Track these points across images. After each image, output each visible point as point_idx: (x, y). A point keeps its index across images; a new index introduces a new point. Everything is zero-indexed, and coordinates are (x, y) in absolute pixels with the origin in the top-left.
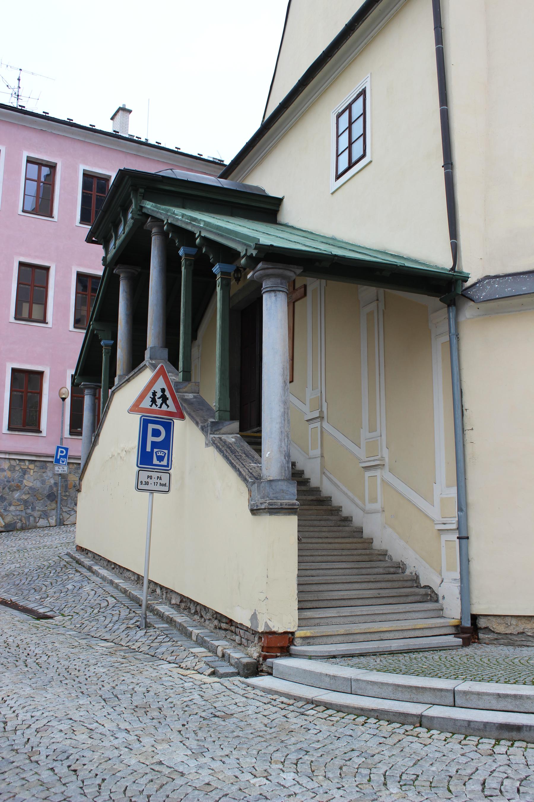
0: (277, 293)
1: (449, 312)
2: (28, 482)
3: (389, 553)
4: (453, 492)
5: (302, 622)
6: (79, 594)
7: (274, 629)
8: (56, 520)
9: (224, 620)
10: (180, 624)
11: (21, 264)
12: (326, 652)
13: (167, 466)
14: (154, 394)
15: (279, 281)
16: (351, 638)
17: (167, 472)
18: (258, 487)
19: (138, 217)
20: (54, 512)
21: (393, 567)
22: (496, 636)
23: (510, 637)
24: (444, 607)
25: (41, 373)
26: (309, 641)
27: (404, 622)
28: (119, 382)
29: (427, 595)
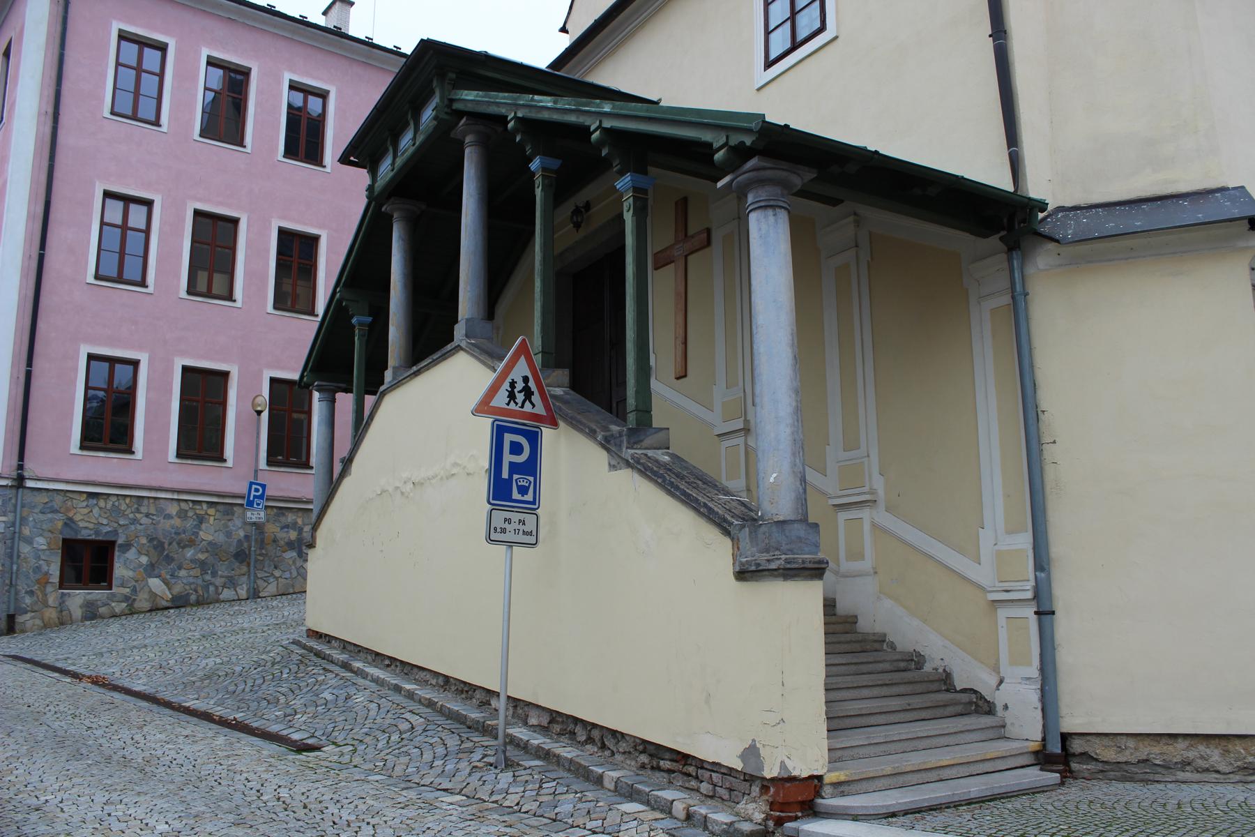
0: (778, 210)
1: (1010, 261)
2: (207, 534)
3: (890, 638)
4: (1024, 541)
5: (836, 756)
6: (350, 709)
7: (795, 773)
8: (248, 590)
9: (667, 756)
10: (571, 761)
11: (197, 213)
12: (882, 807)
13: (534, 503)
14: (513, 384)
15: (778, 190)
16: (901, 780)
17: (533, 512)
18: (750, 533)
19: (446, 117)
20: (244, 579)
21: (903, 660)
22: (1100, 767)
23: (1126, 767)
24: (1008, 722)
25: (226, 375)
26: (842, 789)
27: (955, 746)
28: (394, 379)
29: (971, 703)
